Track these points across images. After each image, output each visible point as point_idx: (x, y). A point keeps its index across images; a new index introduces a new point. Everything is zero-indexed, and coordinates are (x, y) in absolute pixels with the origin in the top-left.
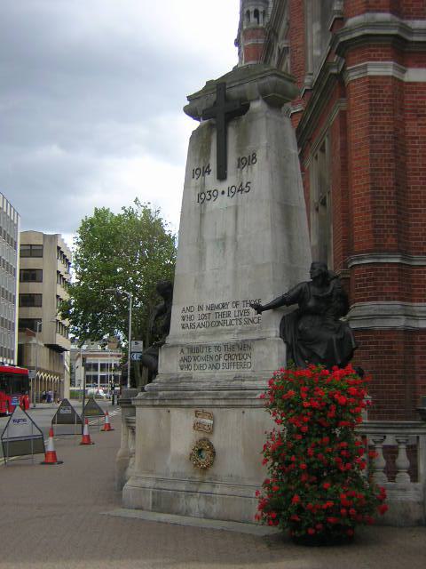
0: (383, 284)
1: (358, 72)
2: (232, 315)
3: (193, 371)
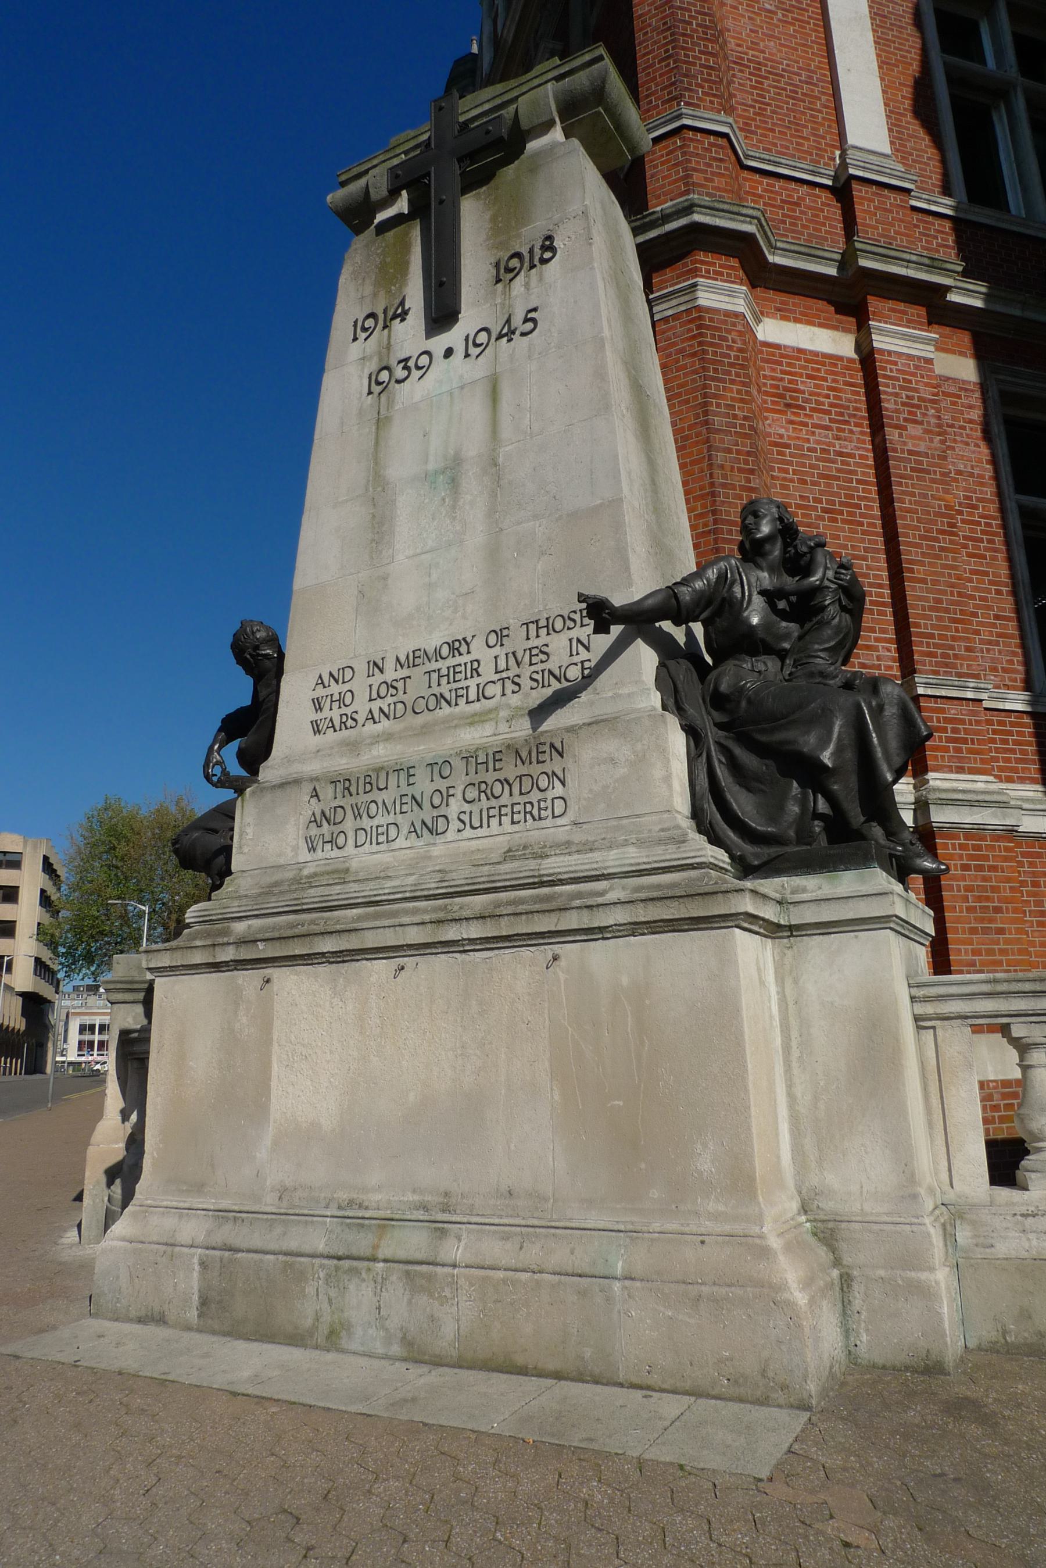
1: (674, 302)
2: (488, 672)
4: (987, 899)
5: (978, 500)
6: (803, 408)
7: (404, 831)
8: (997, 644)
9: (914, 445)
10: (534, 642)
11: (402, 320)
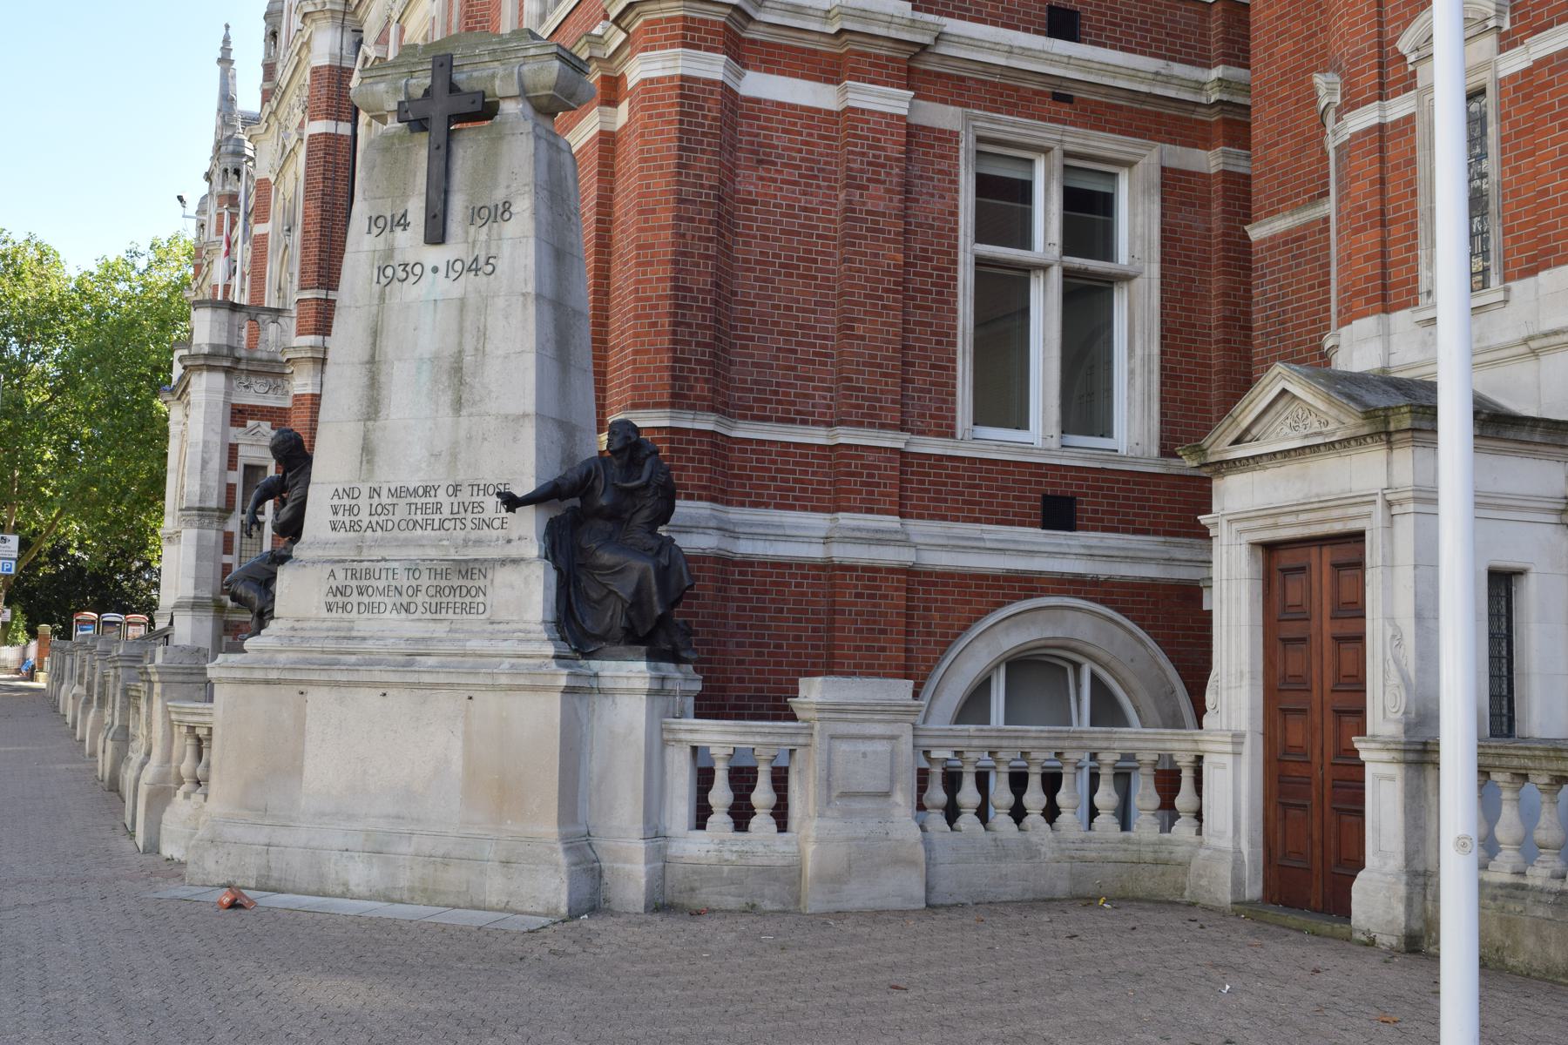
0: (683, 468)
3: (354, 614)
4: (875, 622)
5: (934, 252)
6: (775, 164)
8: (930, 391)
10: (478, 499)
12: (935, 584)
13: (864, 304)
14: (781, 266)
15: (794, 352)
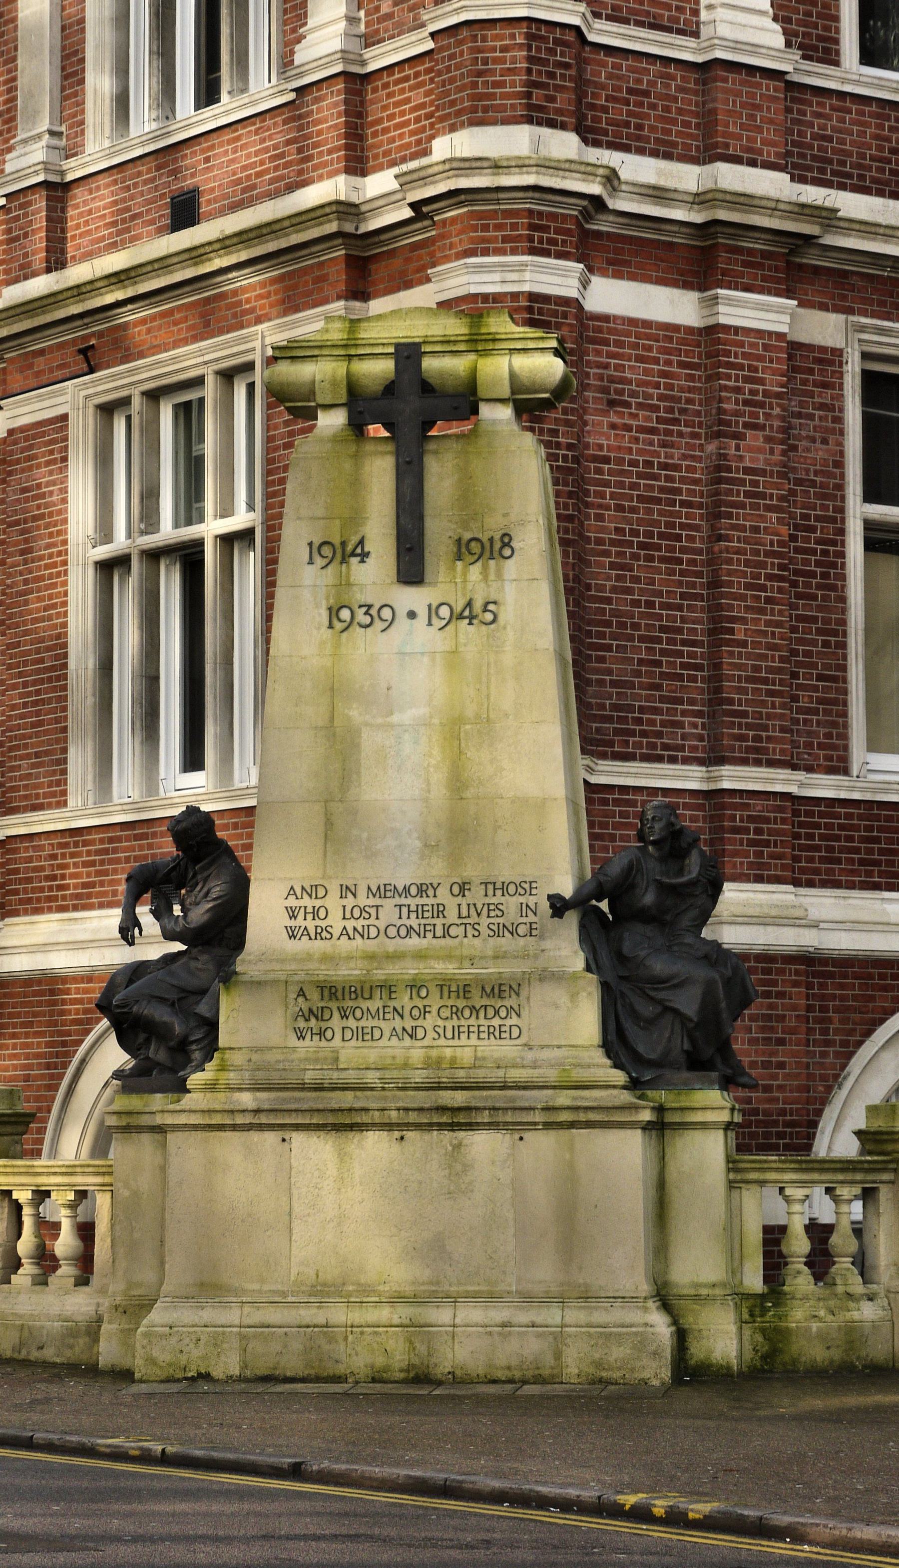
1: (497, 277)
2: (452, 916)
3: (337, 1042)
6: (628, 405)
7: (387, 1034)
9: (752, 460)
10: (494, 900)
11: (362, 561)
12: (831, 975)
13: (743, 598)
14: (641, 546)
15: (658, 664)
